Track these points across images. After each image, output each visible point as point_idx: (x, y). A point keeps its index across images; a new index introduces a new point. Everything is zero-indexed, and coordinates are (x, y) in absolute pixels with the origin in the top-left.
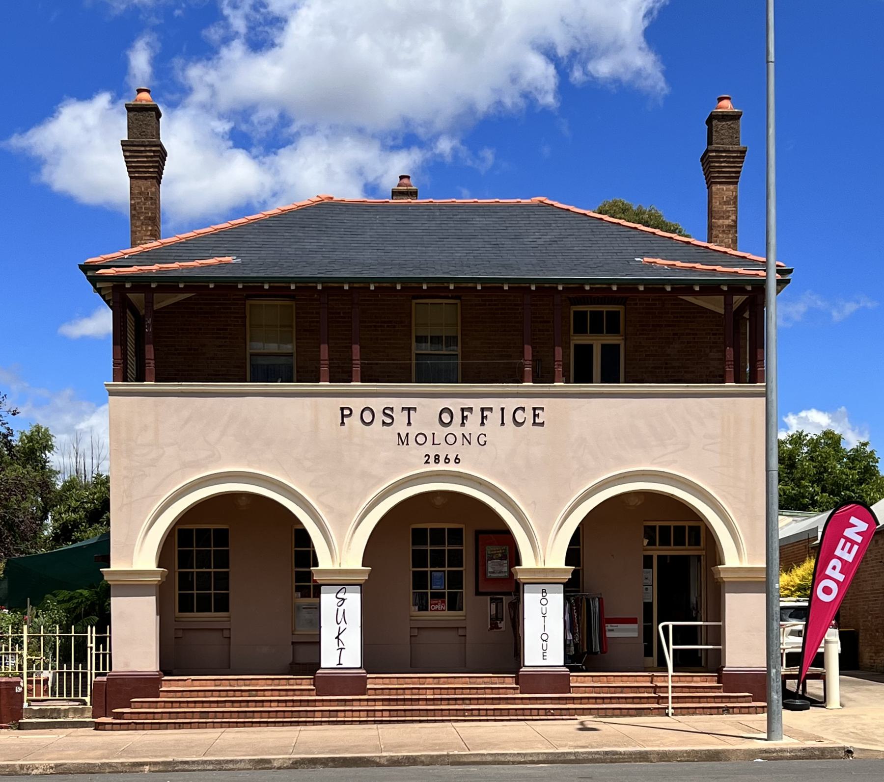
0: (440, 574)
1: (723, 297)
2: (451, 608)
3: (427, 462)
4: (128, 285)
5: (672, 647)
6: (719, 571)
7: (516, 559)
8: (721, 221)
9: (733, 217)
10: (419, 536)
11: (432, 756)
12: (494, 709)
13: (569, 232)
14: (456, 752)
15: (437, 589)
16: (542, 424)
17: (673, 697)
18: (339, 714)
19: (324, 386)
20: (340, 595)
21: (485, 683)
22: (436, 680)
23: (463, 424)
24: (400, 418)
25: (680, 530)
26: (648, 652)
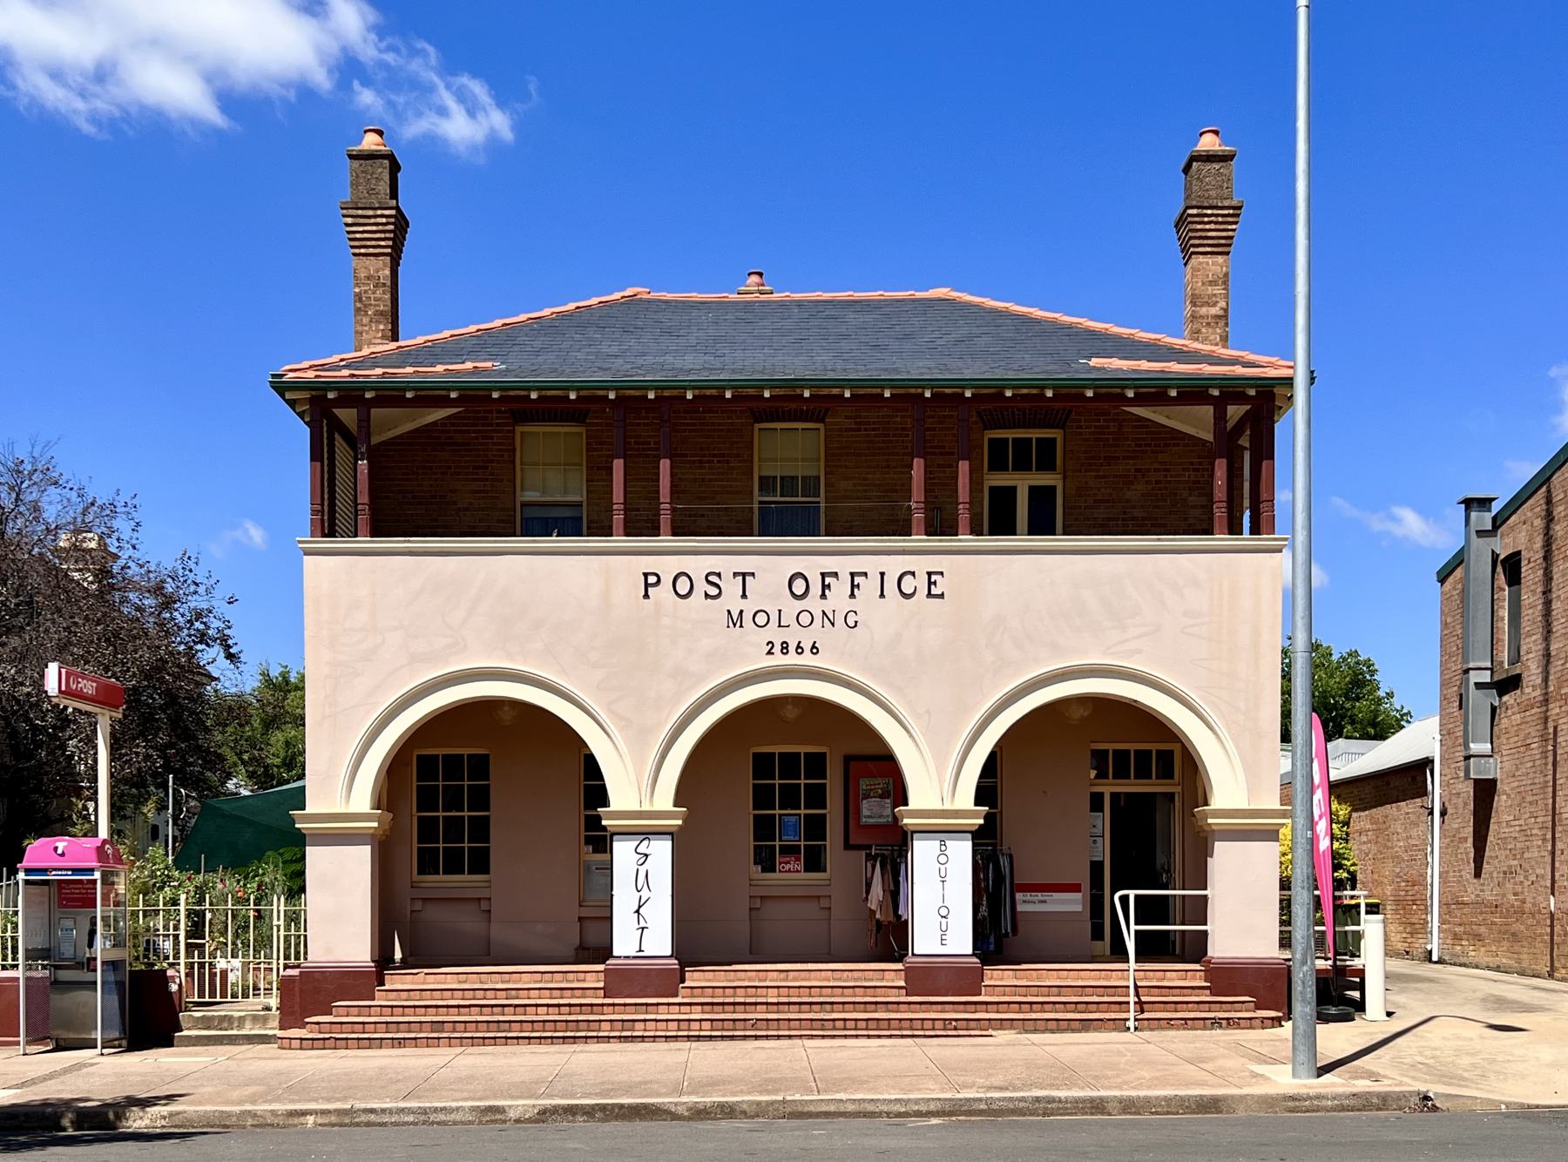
1: (1211, 408)
2: (809, 868)
3: (769, 653)
4: (331, 395)
5: (1133, 927)
6: (1206, 815)
7: (900, 794)
9: (1223, 304)
10: (763, 764)
11: (759, 1103)
13: (986, 330)
14: (797, 1097)
15: (789, 840)
16: (942, 596)
19: (619, 541)
20: (642, 849)
21: (856, 980)
22: (783, 975)
23: (823, 596)
24: (732, 587)
25: (1143, 756)
26: (1097, 934)
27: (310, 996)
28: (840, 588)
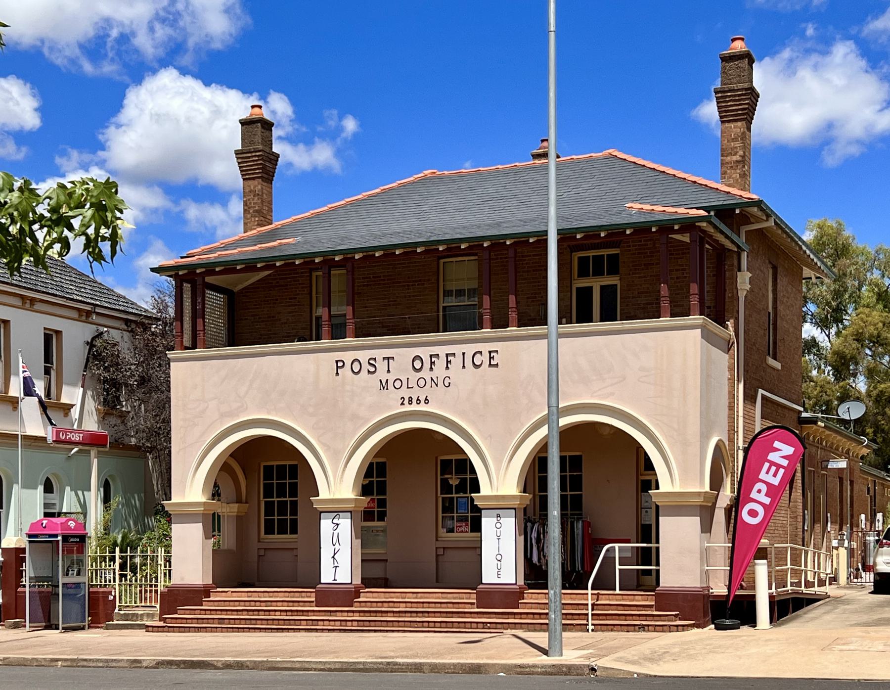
0: (464, 500)
8: (729, 158)
12: (441, 622)
17: (593, 615)
18: (320, 623)
20: (335, 521)
23: (431, 369)
24: (381, 366)
27: (177, 602)
28: (441, 363)
